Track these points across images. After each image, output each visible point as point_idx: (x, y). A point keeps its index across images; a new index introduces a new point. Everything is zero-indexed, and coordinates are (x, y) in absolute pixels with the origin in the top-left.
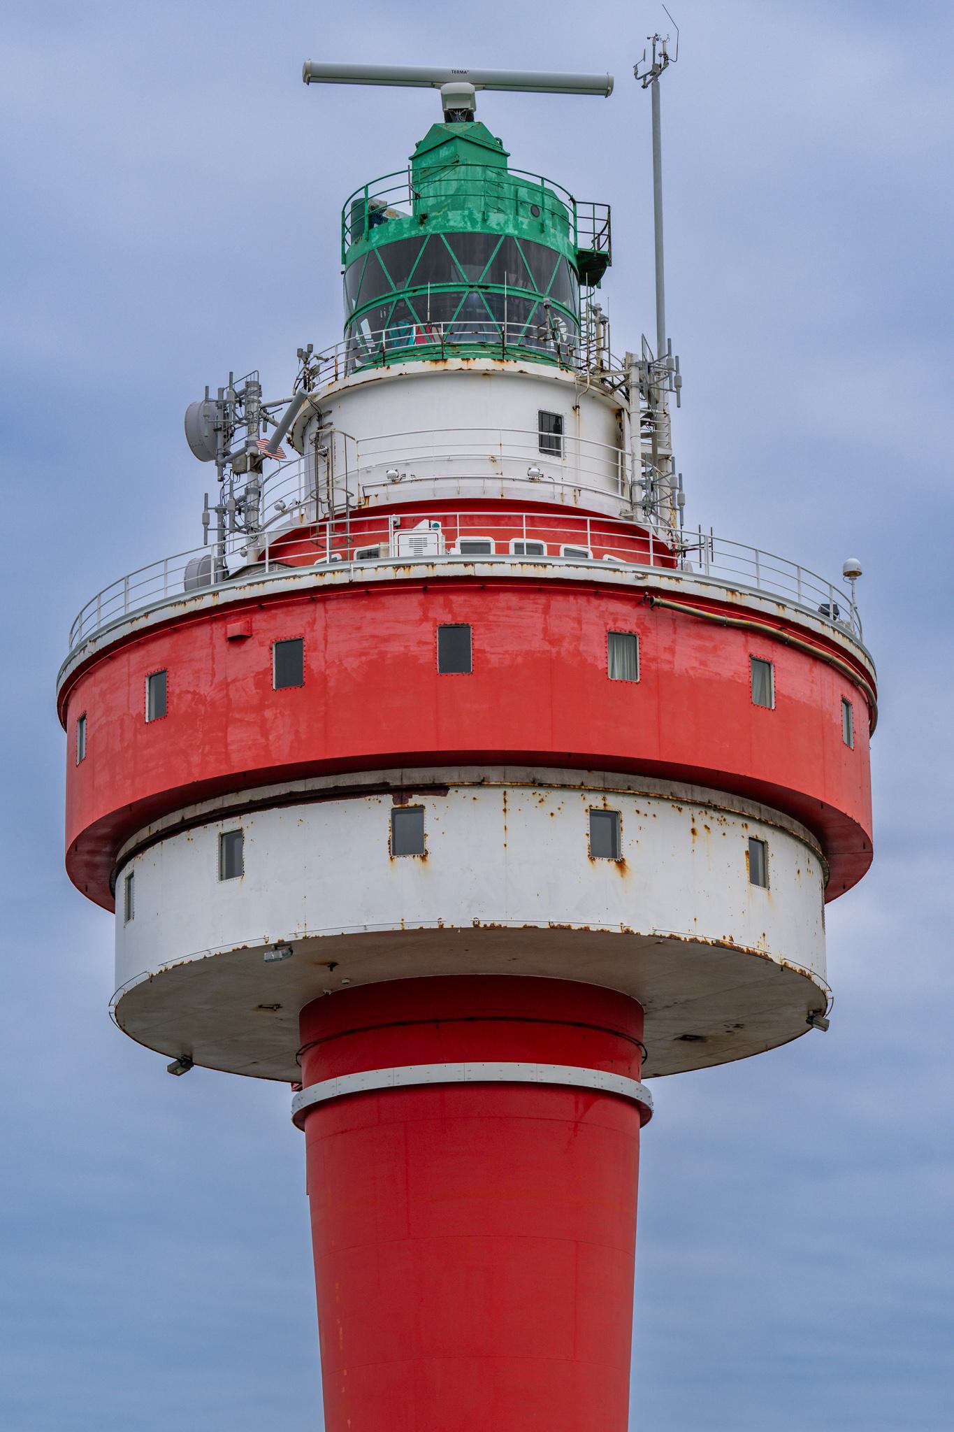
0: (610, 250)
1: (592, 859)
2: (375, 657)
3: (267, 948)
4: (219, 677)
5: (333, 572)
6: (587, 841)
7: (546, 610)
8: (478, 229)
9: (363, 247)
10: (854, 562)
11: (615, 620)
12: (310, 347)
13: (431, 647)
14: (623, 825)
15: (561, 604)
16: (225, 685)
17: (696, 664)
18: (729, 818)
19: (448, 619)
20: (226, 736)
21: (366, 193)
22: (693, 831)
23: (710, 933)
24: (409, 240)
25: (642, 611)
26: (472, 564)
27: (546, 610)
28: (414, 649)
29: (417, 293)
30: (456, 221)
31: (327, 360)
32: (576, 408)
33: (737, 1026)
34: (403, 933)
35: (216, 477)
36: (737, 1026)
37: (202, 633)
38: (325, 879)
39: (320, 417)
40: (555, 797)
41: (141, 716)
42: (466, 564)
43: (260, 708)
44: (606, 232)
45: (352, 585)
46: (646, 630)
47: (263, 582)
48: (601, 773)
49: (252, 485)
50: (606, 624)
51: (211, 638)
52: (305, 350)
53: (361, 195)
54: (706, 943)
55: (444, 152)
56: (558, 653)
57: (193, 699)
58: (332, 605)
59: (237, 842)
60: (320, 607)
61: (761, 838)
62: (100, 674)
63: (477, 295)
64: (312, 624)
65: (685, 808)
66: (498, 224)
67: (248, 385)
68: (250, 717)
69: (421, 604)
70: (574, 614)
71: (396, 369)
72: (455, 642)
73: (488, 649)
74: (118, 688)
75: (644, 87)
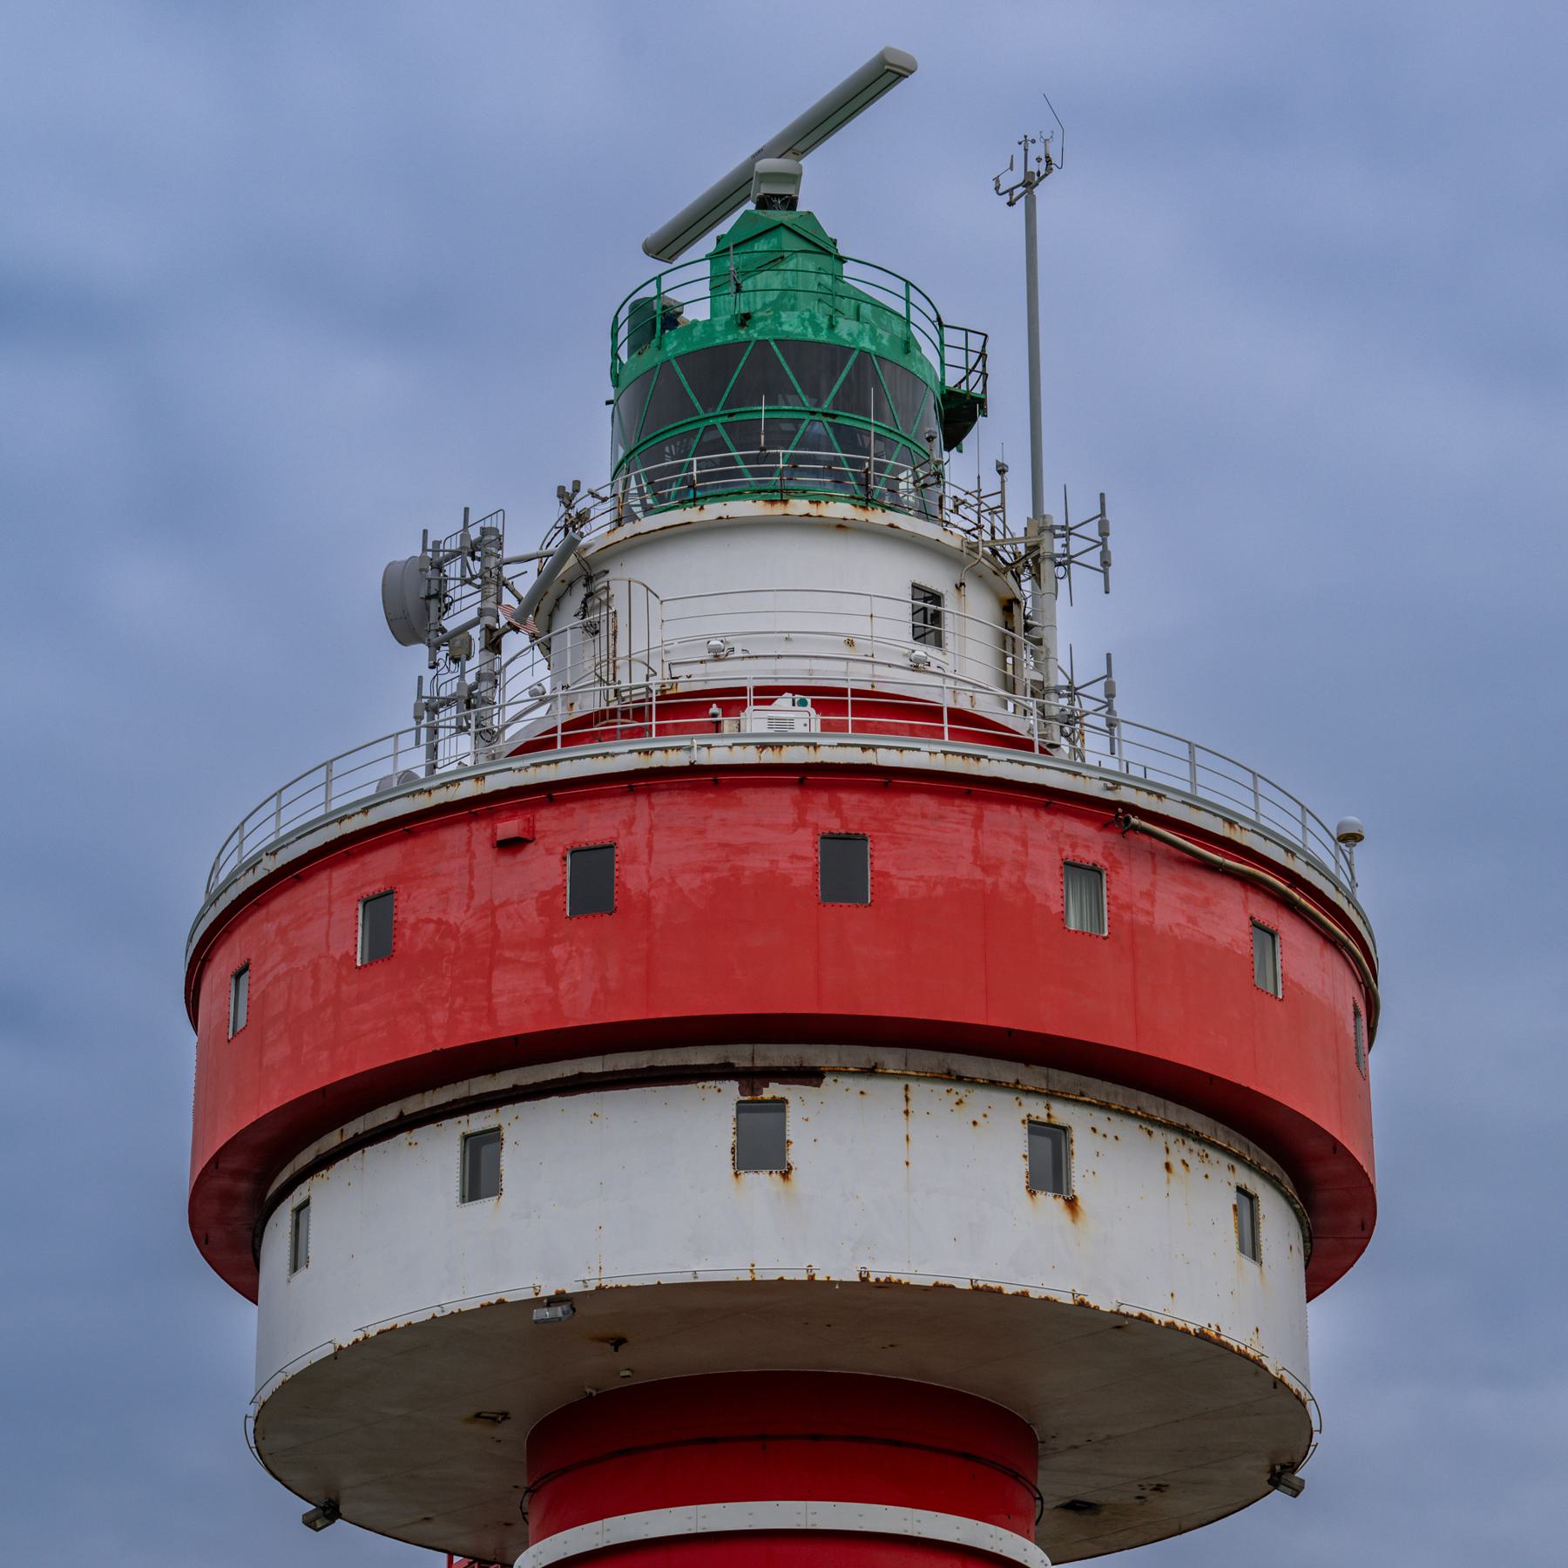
0: (984, 391)
1: (1032, 1193)
2: (725, 874)
3: (537, 1302)
4: (480, 899)
5: (665, 750)
6: (1024, 1166)
7: (978, 822)
8: (823, 337)
9: (651, 358)
10: (1354, 820)
11: (1074, 846)
12: (577, 485)
13: (810, 864)
14: (1075, 1147)
15: (998, 816)
16: (491, 910)
17: (1183, 921)
18: (1214, 1155)
19: (834, 825)
20: (489, 985)
21: (659, 287)
22: (1168, 1166)
23: (1191, 1317)
24: (725, 347)
25: (1111, 837)
26: (874, 748)
27: (978, 822)
28: (785, 866)
29: (734, 418)
30: (792, 325)
31: (604, 500)
32: (960, 586)
33: (1159, 1488)
34: (754, 1286)
35: (426, 662)
36: (1159, 1488)
37: (454, 837)
38: (629, 1202)
39: (589, 579)
40: (979, 1099)
41: (349, 958)
42: (864, 748)
43: (545, 943)
44: (979, 367)
45: (694, 769)
46: (1115, 865)
47: (556, 762)
48: (1044, 1070)
49: (485, 669)
50: (1061, 850)
51: (469, 843)
52: (569, 490)
53: (650, 291)
54: (1185, 1331)
55: (761, 245)
56: (995, 885)
57: (437, 931)
58: (658, 799)
59: (486, 1150)
60: (642, 801)
61: (1251, 1189)
62: (278, 904)
63: (821, 428)
64: (630, 823)
65: (1157, 1131)
66: (850, 334)
67: (484, 531)
68: (528, 956)
69: (795, 803)
70: (1016, 832)
71: (713, 510)
72: (843, 855)
73: (893, 872)
74: (310, 920)
75: (1011, 204)
